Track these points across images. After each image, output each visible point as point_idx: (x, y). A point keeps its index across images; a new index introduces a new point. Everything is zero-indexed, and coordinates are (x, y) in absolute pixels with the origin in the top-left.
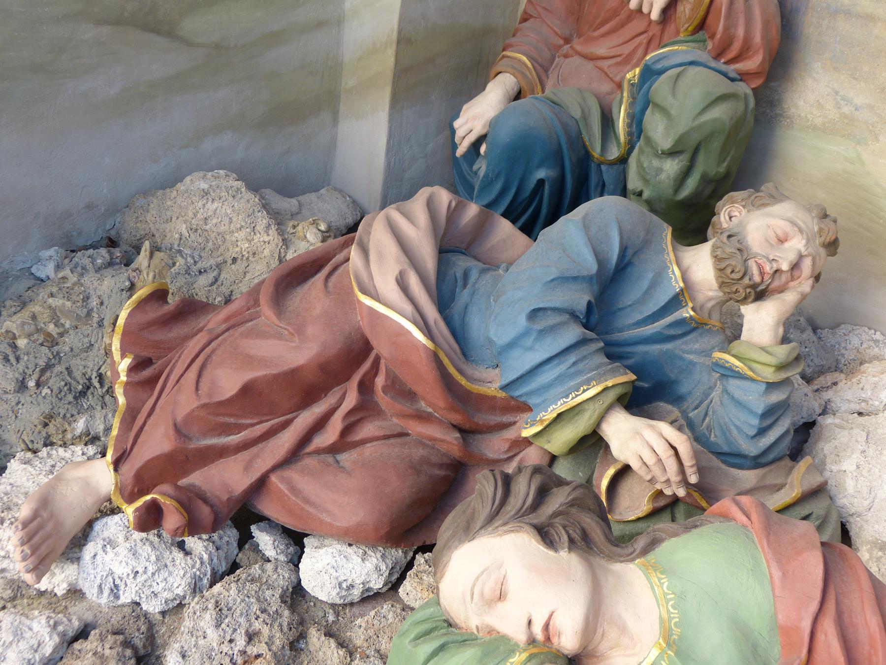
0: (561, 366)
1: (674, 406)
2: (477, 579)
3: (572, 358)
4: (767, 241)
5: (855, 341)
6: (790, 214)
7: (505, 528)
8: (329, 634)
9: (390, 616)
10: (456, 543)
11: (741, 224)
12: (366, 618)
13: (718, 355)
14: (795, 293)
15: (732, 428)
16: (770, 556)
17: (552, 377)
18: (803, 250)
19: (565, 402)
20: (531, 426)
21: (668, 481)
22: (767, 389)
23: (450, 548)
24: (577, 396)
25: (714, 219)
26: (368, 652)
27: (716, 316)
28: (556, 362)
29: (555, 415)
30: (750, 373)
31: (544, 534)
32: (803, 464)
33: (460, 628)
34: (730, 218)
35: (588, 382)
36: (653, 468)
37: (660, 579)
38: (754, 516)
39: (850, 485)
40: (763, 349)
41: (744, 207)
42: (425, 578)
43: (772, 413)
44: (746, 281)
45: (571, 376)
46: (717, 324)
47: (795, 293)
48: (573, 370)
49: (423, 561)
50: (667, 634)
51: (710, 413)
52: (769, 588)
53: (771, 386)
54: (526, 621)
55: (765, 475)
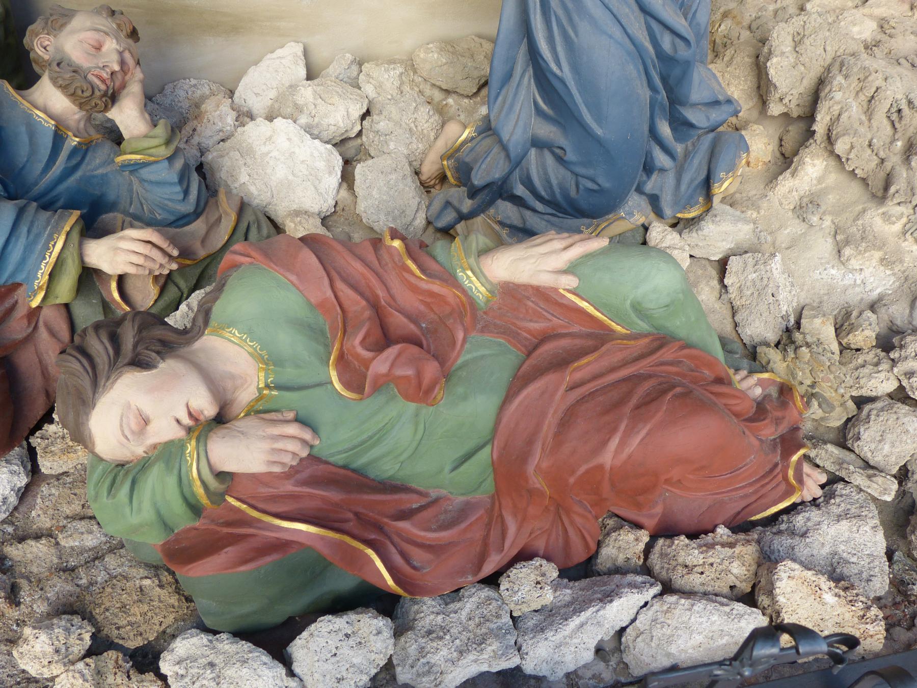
0: (21, 240)
1: (113, 212)
2: (121, 426)
3: (24, 229)
4: (89, 54)
5: (182, 93)
6: (88, 24)
7: (111, 381)
8: (22, 539)
9: (53, 491)
10: (84, 417)
11: (59, 50)
12: (37, 507)
13: (120, 159)
14: (136, 84)
15: (166, 202)
16: (282, 271)
17: (21, 251)
18: (118, 47)
19: (46, 263)
20: (35, 296)
21: (161, 266)
22: (169, 163)
23: (83, 423)
24: (51, 253)
25: (32, 55)
26: (61, 524)
27: (92, 132)
28: (13, 239)
29: (47, 277)
30: (152, 159)
31: (139, 363)
32: (222, 196)
33: (131, 462)
34: (45, 48)
35: (50, 238)
36: (146, 264)
37: (230, 332)
38: (253, 254)
39: (253, 189)
40: (146, 136)
41: (48, 34)
42: (53, 449)
43: (183, 177)
44: (97, 93)
45: (35, 242)
46: (98, 136)
47: (136, 84)
48: (31, 237)
49: (39, 440)
50: (259, 358)
51: (143, 201)
52: (294, 289)
53: (171, 159)
54: (175, 423)
55: (207, 217)
